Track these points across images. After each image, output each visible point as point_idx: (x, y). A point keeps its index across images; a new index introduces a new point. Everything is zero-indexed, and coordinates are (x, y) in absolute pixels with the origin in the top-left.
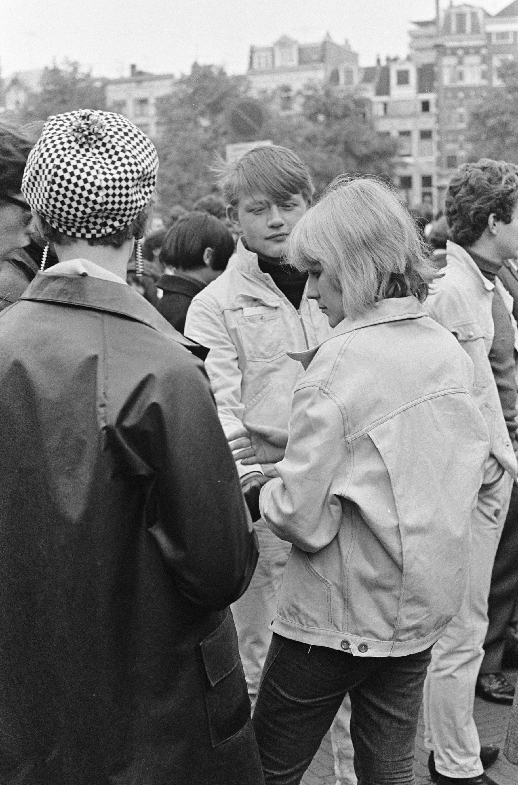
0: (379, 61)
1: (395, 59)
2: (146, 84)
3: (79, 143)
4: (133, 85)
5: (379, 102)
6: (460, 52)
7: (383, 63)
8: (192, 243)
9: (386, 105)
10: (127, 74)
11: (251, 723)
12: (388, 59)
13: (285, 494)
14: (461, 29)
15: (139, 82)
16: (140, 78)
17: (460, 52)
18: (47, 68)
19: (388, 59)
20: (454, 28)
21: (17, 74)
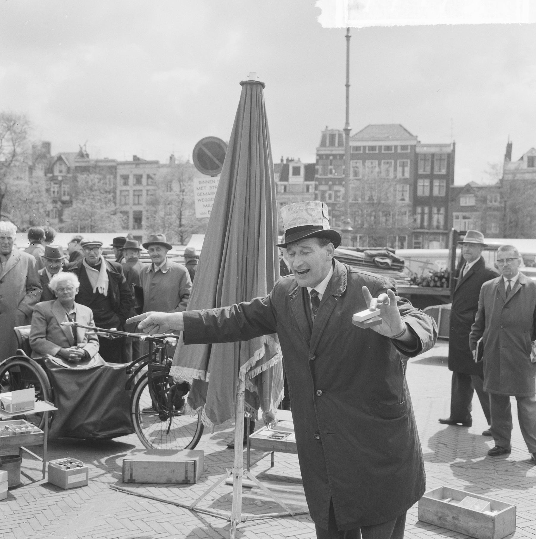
0: (282, 160)
1: (292, 160)
2: (141, 166)
3: (153, 209)
4: (134, 166)
5: (281, 185)
6: (331, 158)
7: (285, 162)
8: (514, 338)
9: (285, 187)
10: (131, 159)
11: (32, 427)
12: (288, 160)
13: (200, 371)
14: (332, 143)
15: (137, 164)
16: (138, 162)
17: (331, 158)
18: (47, 145)
19: (288, 160)
20: (328, 144)
21: (61, 154)
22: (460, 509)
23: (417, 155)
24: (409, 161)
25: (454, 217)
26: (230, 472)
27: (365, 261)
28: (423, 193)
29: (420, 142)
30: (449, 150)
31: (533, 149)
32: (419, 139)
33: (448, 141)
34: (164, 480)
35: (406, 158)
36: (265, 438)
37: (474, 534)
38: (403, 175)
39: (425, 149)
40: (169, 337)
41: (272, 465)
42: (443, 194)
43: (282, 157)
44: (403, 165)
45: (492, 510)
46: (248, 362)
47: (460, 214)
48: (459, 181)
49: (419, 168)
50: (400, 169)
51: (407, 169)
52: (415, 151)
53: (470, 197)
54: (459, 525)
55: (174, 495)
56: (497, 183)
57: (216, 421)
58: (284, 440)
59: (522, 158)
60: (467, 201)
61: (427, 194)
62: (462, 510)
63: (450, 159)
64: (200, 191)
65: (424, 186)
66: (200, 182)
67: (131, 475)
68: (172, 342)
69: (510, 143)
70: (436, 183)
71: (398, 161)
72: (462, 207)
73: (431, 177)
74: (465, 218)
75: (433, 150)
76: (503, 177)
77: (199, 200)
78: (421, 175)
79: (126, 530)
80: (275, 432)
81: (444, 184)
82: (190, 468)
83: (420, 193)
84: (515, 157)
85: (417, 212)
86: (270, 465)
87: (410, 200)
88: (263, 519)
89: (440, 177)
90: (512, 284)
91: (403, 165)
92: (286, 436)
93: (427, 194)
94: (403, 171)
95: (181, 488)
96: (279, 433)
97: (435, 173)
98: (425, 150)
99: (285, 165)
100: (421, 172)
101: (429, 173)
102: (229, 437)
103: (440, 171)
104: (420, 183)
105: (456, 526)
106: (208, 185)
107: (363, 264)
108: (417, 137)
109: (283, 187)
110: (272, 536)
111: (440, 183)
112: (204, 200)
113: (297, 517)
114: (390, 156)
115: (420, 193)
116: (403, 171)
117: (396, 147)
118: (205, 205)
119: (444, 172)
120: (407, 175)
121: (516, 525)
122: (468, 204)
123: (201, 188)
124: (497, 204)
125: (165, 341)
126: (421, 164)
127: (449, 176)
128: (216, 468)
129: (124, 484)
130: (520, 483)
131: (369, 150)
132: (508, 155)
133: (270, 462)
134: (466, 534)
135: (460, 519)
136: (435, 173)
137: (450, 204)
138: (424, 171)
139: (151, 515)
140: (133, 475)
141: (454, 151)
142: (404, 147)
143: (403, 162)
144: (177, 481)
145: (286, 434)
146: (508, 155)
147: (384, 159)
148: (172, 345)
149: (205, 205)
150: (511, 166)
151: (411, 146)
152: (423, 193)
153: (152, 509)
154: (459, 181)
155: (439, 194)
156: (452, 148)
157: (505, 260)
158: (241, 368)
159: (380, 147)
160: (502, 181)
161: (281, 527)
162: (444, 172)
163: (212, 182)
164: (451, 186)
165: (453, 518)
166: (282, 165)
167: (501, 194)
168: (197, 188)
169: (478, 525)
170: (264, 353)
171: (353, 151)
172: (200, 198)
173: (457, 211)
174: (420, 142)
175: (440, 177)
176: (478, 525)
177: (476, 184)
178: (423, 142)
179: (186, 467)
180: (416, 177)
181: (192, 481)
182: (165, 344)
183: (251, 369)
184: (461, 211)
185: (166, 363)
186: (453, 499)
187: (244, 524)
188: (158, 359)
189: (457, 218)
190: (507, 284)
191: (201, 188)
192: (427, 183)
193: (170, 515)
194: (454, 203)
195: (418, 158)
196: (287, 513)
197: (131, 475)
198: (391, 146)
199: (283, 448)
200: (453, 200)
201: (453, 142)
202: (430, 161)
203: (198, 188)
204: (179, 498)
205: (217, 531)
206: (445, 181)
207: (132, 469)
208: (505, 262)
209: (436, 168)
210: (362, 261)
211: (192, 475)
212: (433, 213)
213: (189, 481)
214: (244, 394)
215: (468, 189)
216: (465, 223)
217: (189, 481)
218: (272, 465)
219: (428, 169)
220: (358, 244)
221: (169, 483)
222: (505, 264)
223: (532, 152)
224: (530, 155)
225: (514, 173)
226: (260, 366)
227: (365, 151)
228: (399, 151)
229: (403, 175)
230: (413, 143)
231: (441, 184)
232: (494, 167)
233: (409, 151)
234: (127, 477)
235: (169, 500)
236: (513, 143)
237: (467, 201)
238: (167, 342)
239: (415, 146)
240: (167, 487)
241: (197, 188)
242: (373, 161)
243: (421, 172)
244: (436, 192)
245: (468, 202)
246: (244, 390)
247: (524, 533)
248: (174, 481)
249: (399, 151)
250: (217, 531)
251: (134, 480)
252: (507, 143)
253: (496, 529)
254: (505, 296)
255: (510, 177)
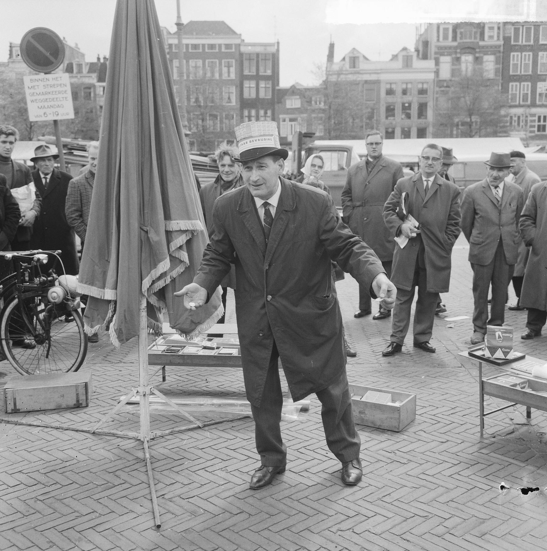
0: (99, 59)
5: (100, 86)
22: (366, 404)
23: (241, 54)
24: (234, 61)
25: (281, 120)
26: (136, 391)
27: (210, 166)
28: (250, 95)
29: (243, 40)
30: (273, 49)
31: (354, 49)
32: (243, 38)
33: (272, 40)
34: (52, 406)
35: (231, 59)
36: (160, 353)
37: (380, 425)
38: (229, 76)
39: (250, 48)
40: (38, 253)
41: (164, 379)
42: (269, 96)
43: (99, 55)
44: (229, 66)
45: (393, 401)
46: (149, 275)
47: (287, 117)
48: (285, 82)
49: (244, 69)
50: (225, 70)
51: (233, 70)
52: (240, 51)
53: (295, 99)
54: (365, 418)
55: (68, 420)
56: (321, 85)
57: (122, 340)
58: (180, 353)
59: (344, 59)
60: (293, 103)
61: (253, 95)
62: (368, 404)
63: (274, 59)
64: (32, 91)
65: (250, 87)
66: (31, 80)
67: (15, 404)
68: (43, 260)
69: (332, 43)
70: (262, 84)
71: (223, 61)
72: (288, 109)
73: (257, 78)
74: (291, 120)
75: (258, 49)
76: (327, 78)
77: (32, 101)
78: (246, 75)
79: (26, 462)
80: (168, 346)
81: (270, 85)
82: (82, 391)
83: (246, 95)
84: (337, 58)
85: (244, 116)
86: (161, 380)
87: (236, 102)
88: (172, 435)
89: (266, 78)
90: (430, 184)
91: (229, 66)
92: (182, 349)
93: (253, 95)
94: (229, 72)
95: (74, 413)
96: (173, 346)
97: (261, 74)
98: (249, 49)
99: (102, 64)
100: (246, 72)
101: (255, 74)
102: (108, 355)
103: (265, 72)
104: (246, 84)
105: (362, 420)
106: (41, 84)
107: (207, 169)
108: (240, 35)
109: (102, 89)
110: (187, 450)
111: (265, 84)
112: (38, 101)
113: (206, 428)
114: (214, 55)
115: (246, 95)
116: (229, 72)
117: (220, 46)
118: (40, 107)
119: (269, 72)
120: (233, 76)
121: (417, 413)
122: (294, 107)
123: (33, 87)
124: (322, 105)
125: (35, 259)
126: (246, 64)
127: (274, 78)
128: (105, 388)
129: (7, 415)
130: (405, 373)
131: (208, 49)
132: (331, 56)
133: (162, 376)
134: (372, 426)
135: (366, 412)
136: (261, 74)
137: (276, 106)
138: (250, 72)
139: (49, 443)
140: (17, 404)
141: (278, 50)
142: (228, 46)
143: (228, 62)
144: (67, 405)
145: (180, 347)
146: (331, 56)
147: (208, 59)
148: (43, 263)
149: (40, 107)
150: (336, 67)
151: (236, 45)
152: (250, 95)
153: (49, 438)
154: (285, 82)
155: (266, 96)
156: (276, 47)
157: (431, 158)
158: (143, 282)
159: (204, 45)
160: (325, 82)
161: (193, 440)
162: (269, 72)
163: (45, 80)
164: (277, 88)
165: (360, 412)
166: (99, 64)
167: (326, 96)
168: (29, 87)
169: (384, 416)
170: (170, 264)
171: (192, 49)
172: (33, 98)
173: (284, 113)
174: (243, 40)
175: (266, 78)
176: (384, 416)
177: (301, 85)
178: (246, 41)
179: (76, 390)
180: (242, 78)
181: (84, 404)
182: (37, 262)
183: (153, 282)
184: (287, 114)
185: (38, 283)
186: (354, 395)
187: (154, 441)
188: (27, 279)
189: (284, 121)
190: (425, 183)
191: (33, 87)
192: (253, 84)
193: (71, 441)
194: (280, 105)
195: (243, 58)
196: (196, 426)
197: (15, 404)
198: (215, 45)
199: (181, 361)
200: (279, 102)
201: (276, 41)
202: (255, 61)
203: (30, 87)
204: (74, 423)
205: (127, 452)
206: (270, 82)
207: (15, 399)
208: (431, 160)
209: (261, 69)
210: (206, 166)
211: (84, 398)
212: (260, 115)
213: (81, 404)
214: (146, 310)
215: (294, 91)
216: (292, 125)
217: (81, 404)
218: (164, 379)
219: (254, 69)
220: (196, 149)
221: (58, 409)
222: (430, 162)
223: (353, 53)
224: (351, 55)
225: (339, 73)
226: (164, 279)
227: (205, 49)
228: (223, 50)
229: (229, 76)
230: (238, 41)
231: (268, 86)
232: (319, 68)
233: (233, 50)
234: (10, 407)
235: (65, 426)
236: (335, 42)
237: (293, 103)
238: (39, 259)
239: (239, 45)
240: (58, 413)
241: (29, 87)
242: (197, 60)
243: (246, 72)
244: (262, 95)
245: (293, 104)
246: (146, 305)
247: (424, 419)
248: (64, 406)
249: (223, 50)
250: (127, 452)
251: (19, 410)
252: (329, 43)
253: (402, 417)
254: (425, 195)
255: (334, 78)
